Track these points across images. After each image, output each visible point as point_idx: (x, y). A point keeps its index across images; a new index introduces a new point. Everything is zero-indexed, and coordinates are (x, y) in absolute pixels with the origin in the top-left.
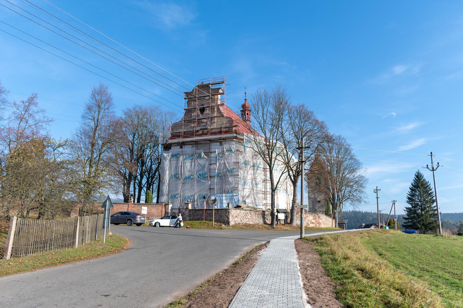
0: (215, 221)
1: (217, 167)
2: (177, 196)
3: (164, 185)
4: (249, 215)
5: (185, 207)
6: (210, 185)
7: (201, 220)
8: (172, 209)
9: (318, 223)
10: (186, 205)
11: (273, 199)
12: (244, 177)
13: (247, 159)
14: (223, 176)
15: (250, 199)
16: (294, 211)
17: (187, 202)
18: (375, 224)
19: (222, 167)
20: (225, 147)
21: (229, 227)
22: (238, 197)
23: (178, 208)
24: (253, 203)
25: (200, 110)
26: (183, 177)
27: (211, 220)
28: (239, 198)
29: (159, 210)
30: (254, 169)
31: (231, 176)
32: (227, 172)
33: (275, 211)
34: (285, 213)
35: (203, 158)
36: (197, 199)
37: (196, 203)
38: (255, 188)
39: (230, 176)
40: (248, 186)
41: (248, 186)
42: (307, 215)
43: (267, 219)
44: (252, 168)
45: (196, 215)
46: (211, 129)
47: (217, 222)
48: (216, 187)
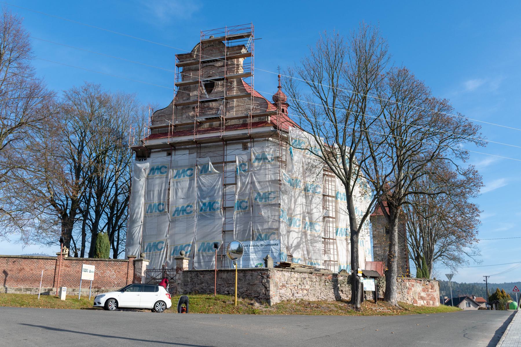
0: (239, 297)
1: (238, 190)
2: (159, 247)
3: (136, 225)
4: (308, 282)
5: (175, 267)
6: (225, 224)
7: (209, 294)
8: (148, 271)
9: (432, 297)
10: (178, 261)
11: (355, 250)
12: (289, 209)
13: (294, 176)
14: (249, 206)
15: (301, 252)
16: (392, 274)
17: (179, 256)
18: (468, 298)
19: (247, 190)
20: (253, 153)
21: (269, 309)
22: (279, 247)
23: (161, 267)
24: (305, 260)
25: (206, 85)
26: (173, 209)
27: (230, 293)
28: (282, 249)
29: (122, 273)
30: (306, 197)
31: (265, 206)
32: (258, 199)
33: (360, 274)
34: (375, 278)
35: (211, 173)
36: (199, 251)
37: (195, 259)
38: (309, 232)
39: (263, 208)
40: (297, 227)
41: (296, 227)
42: (413, 283)
43: (342, 291)
44: (303, 192)
45: (199, 282)
46: (226, 120)
47: (243, 298)
48: (236, 228)
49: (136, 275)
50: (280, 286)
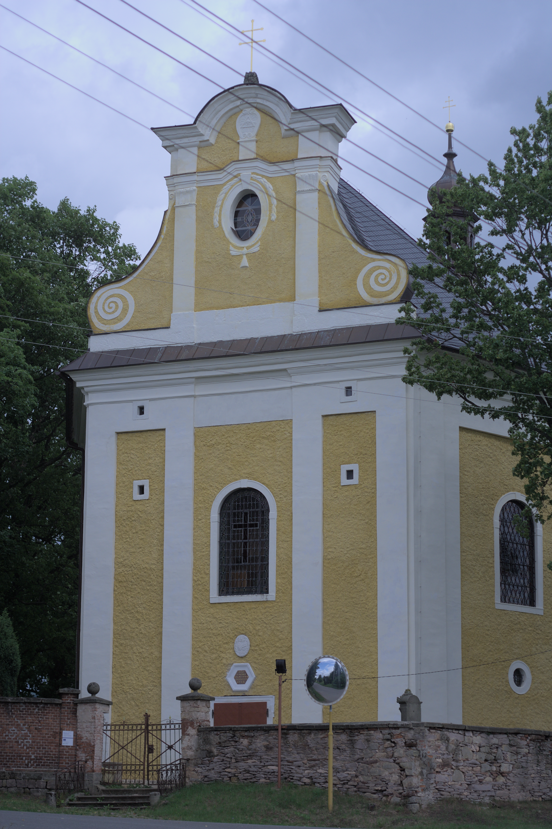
49: (81, 738)
50: (439, 766)
